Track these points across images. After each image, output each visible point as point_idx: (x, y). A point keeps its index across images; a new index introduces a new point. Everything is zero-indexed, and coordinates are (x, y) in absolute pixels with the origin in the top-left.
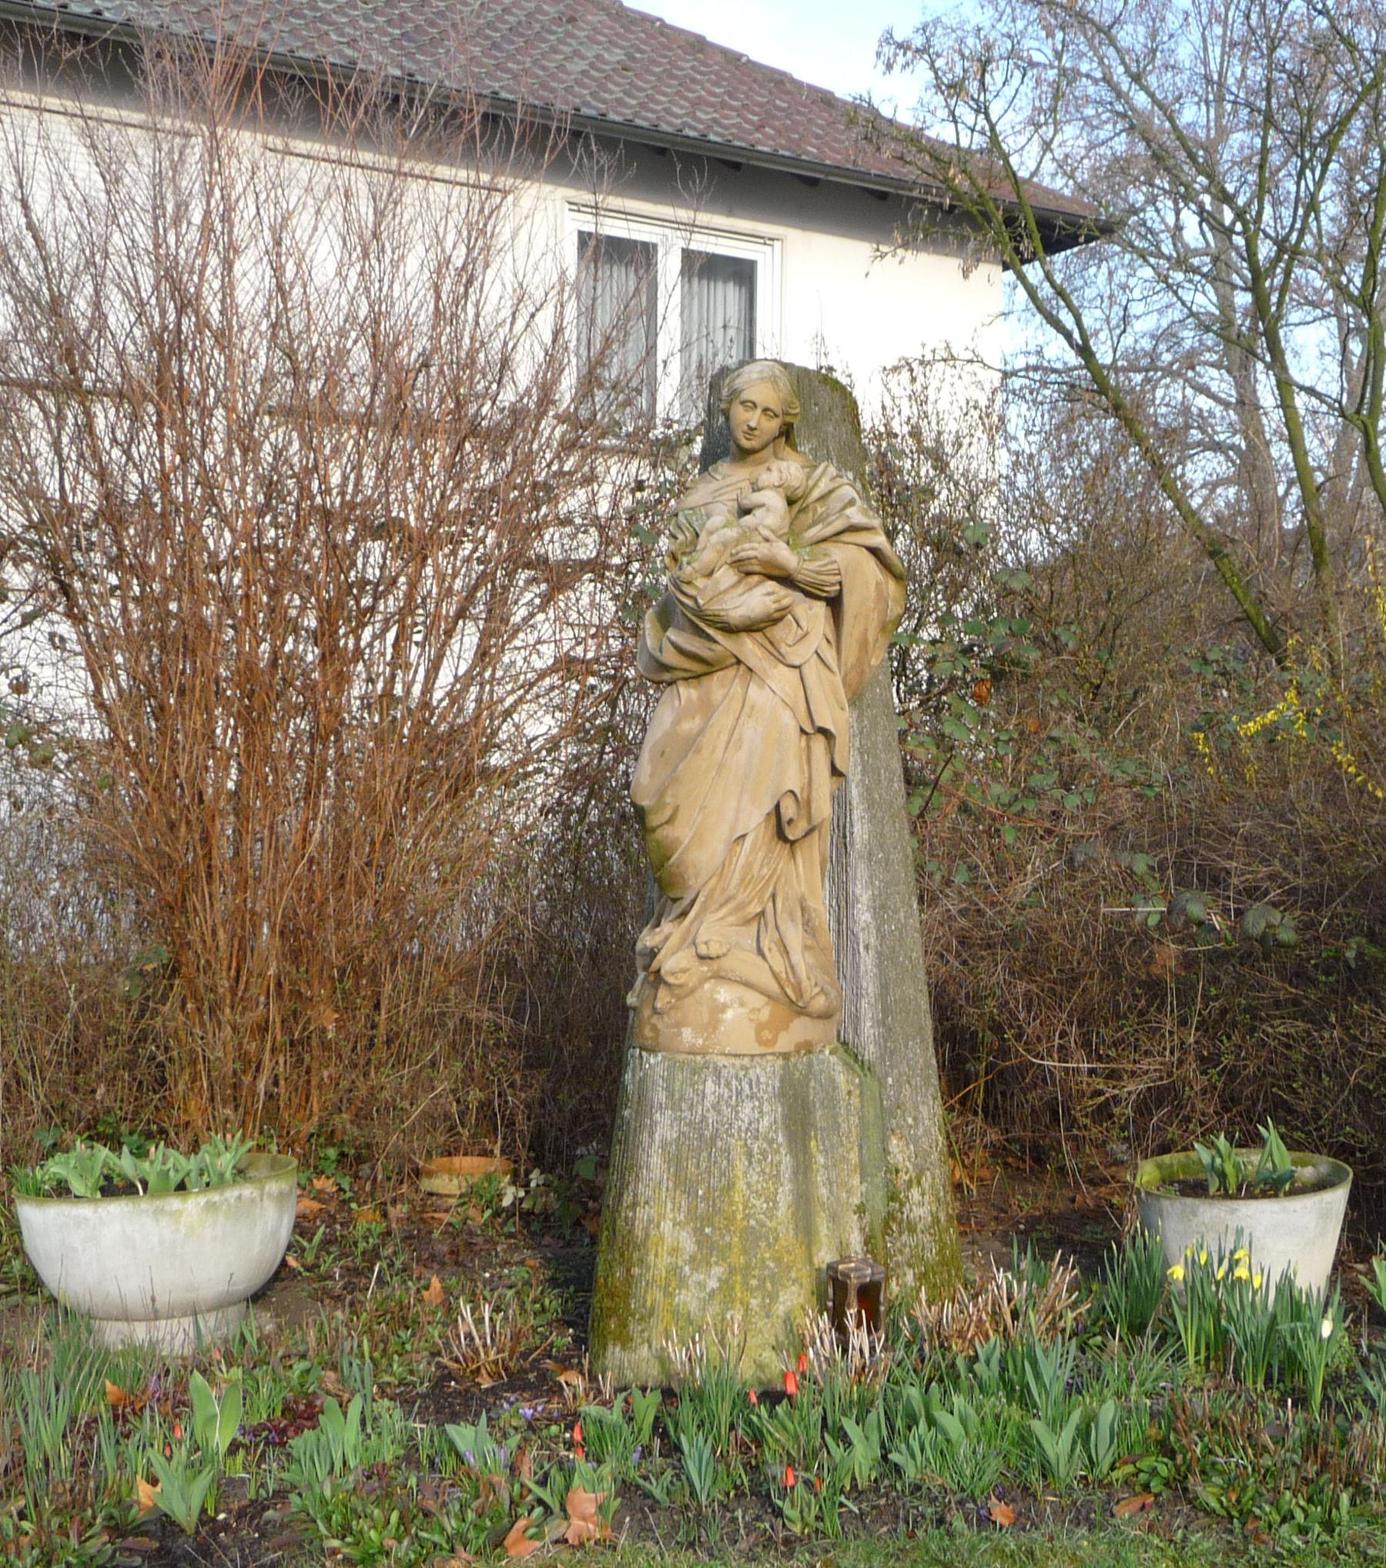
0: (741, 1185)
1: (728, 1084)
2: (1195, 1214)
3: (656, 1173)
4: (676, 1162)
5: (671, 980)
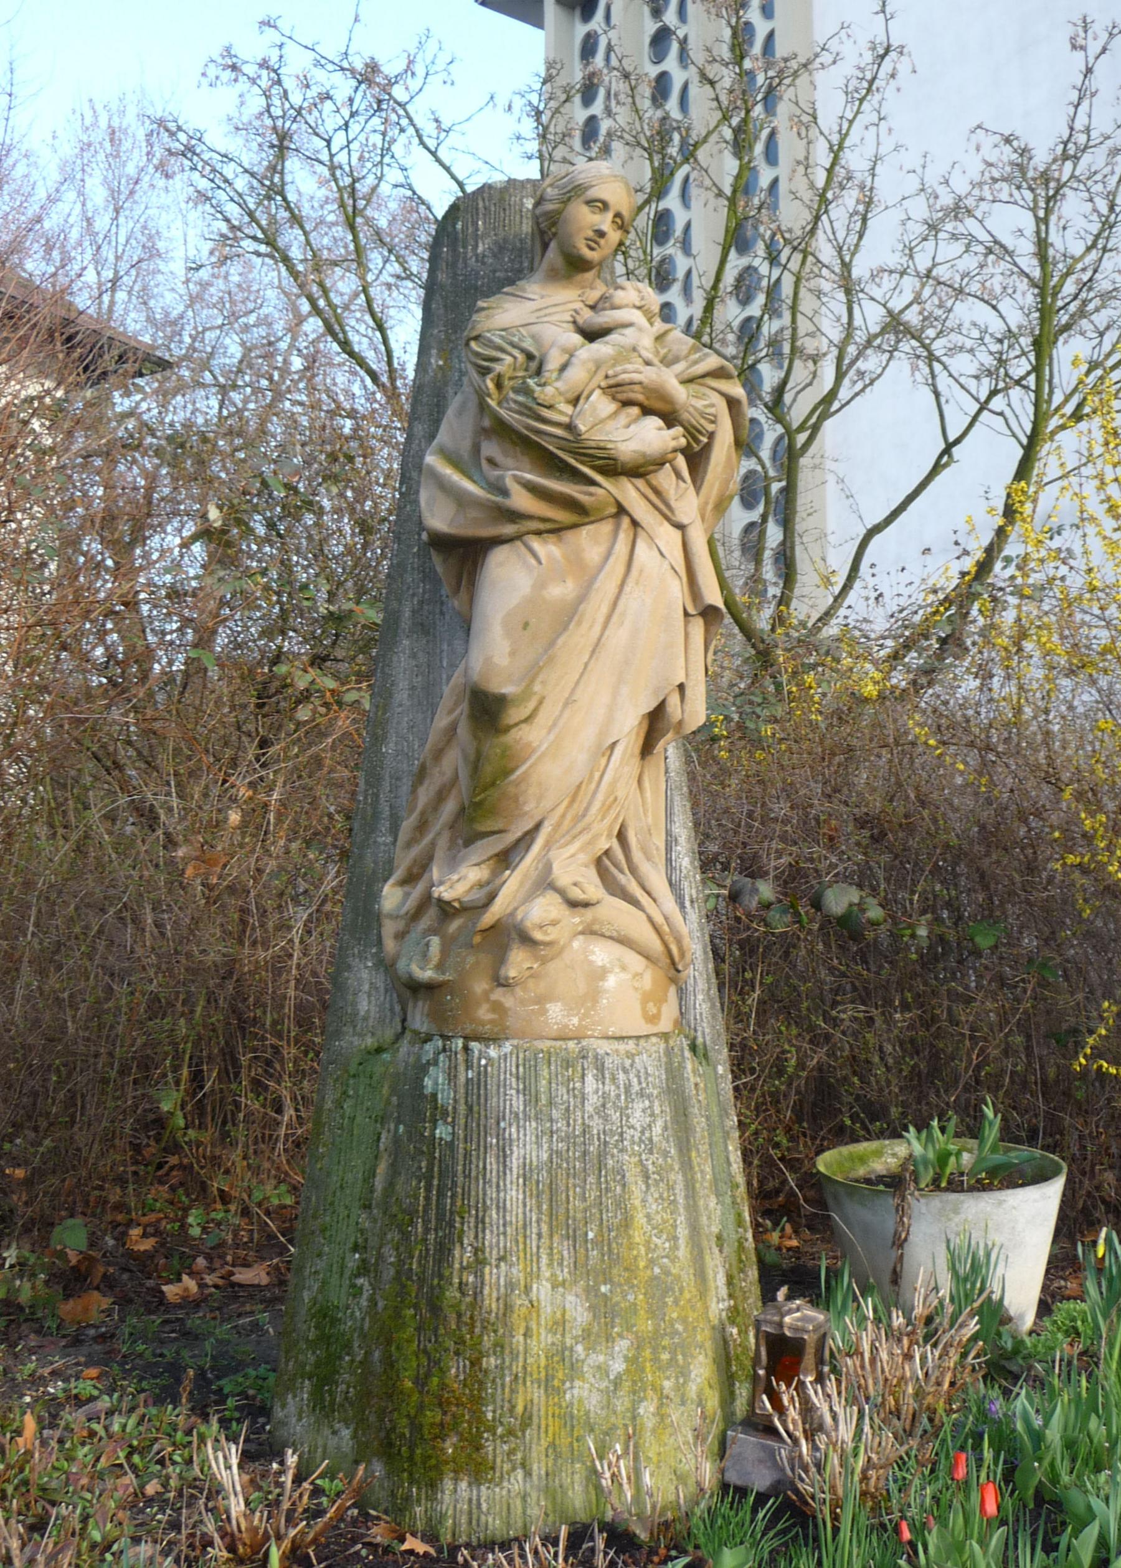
0: (640, 1219)
1: (614, 1079)
2: (956, 1211)
3: (515, 1214)
4: (548, 1191)
5: (538, 936)
